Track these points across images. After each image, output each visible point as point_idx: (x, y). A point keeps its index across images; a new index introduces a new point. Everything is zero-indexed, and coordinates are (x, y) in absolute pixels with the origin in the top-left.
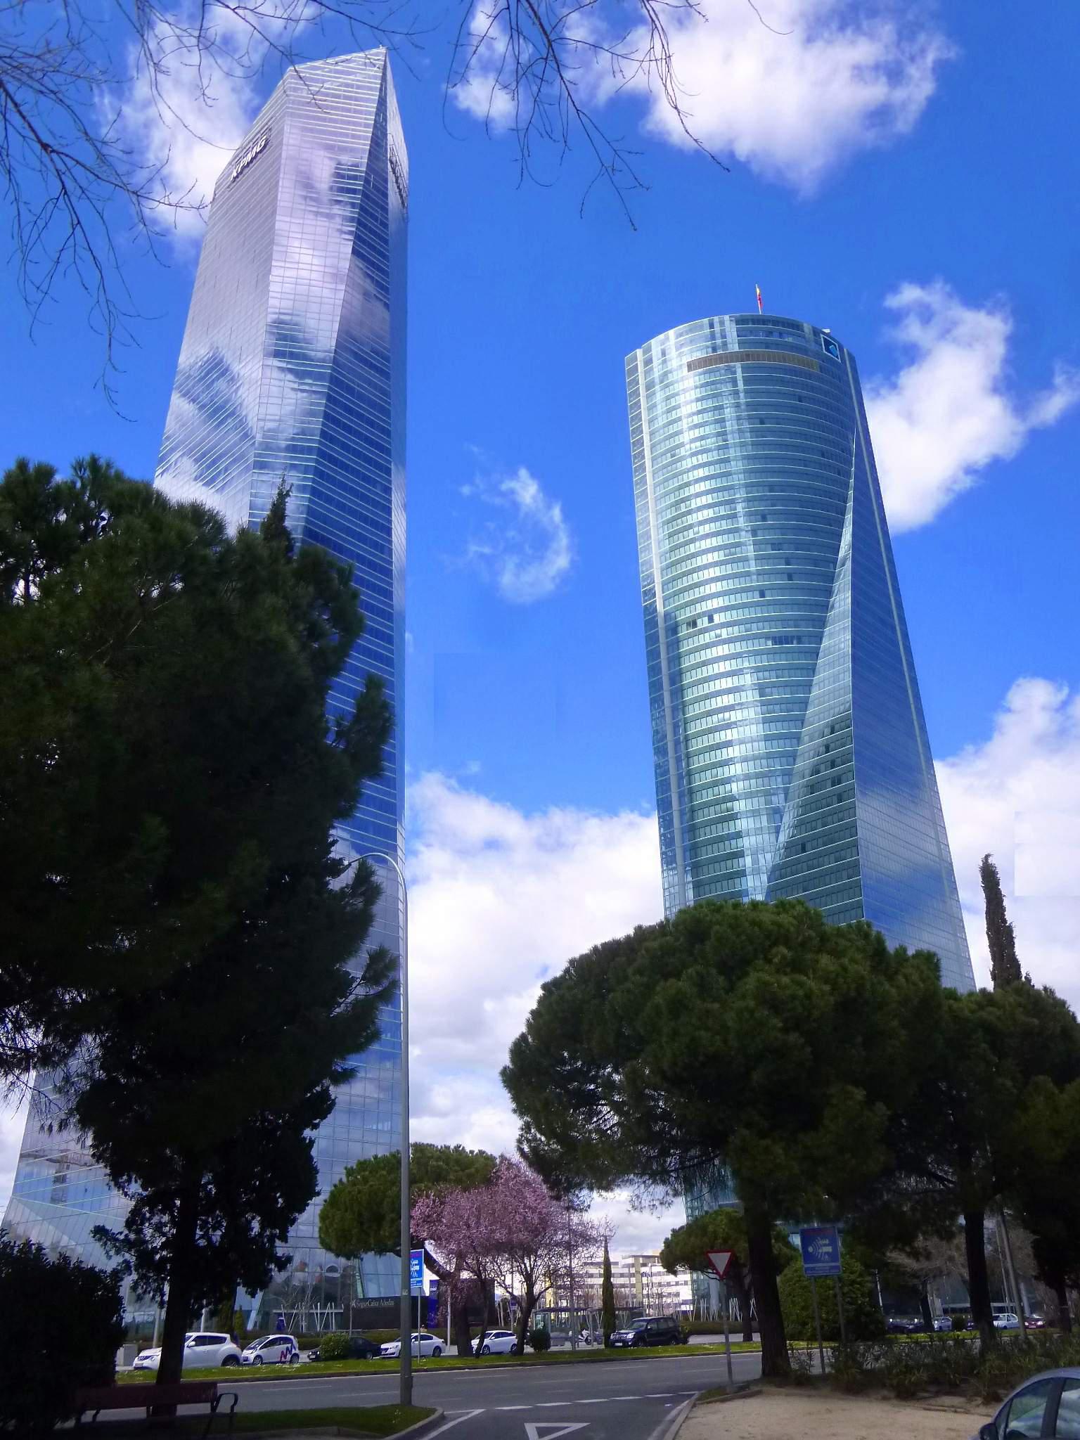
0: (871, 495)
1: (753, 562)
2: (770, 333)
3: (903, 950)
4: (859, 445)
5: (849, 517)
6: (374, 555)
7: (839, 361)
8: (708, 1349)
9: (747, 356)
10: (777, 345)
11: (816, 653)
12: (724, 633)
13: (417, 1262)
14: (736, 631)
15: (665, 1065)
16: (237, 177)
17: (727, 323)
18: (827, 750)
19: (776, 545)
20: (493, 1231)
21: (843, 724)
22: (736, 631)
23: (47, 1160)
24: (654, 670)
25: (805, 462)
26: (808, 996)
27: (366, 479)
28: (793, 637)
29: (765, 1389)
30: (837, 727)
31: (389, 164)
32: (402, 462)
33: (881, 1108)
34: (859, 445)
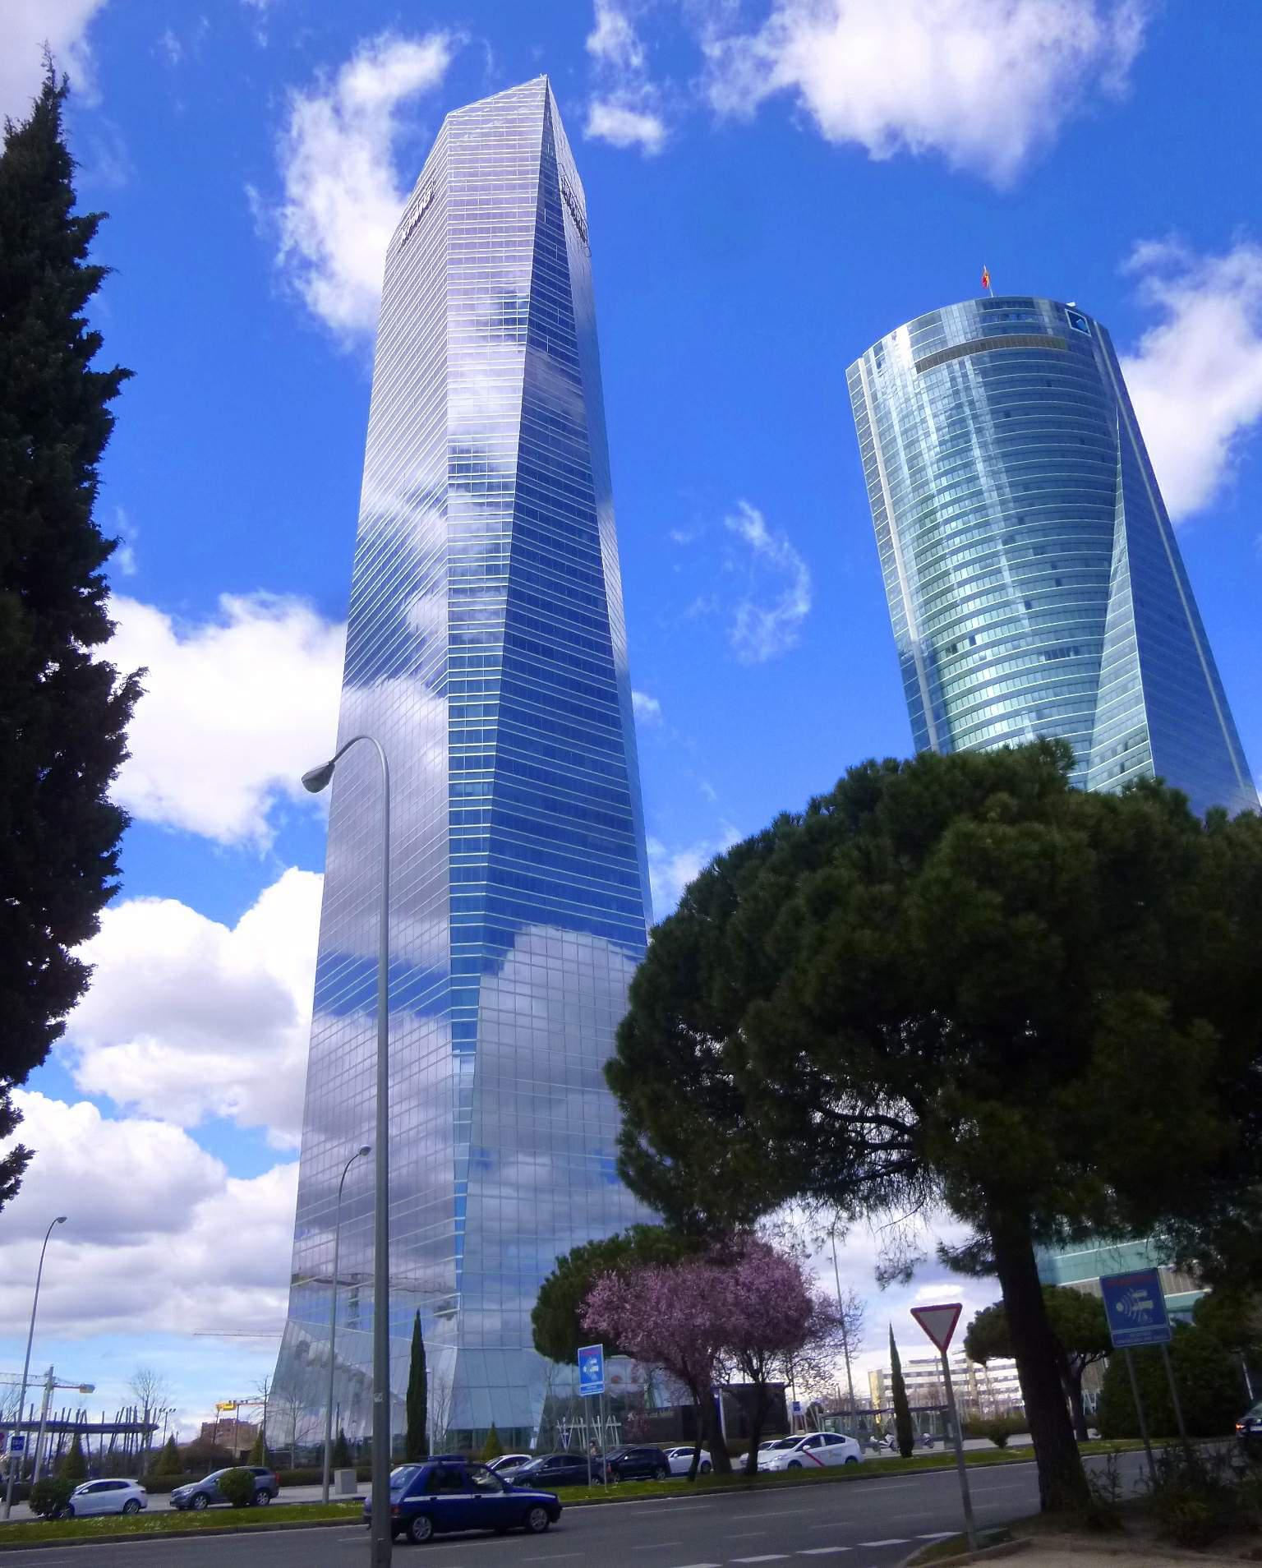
0: (1138, 465)
1: (1026, 622)
2: (1006, 316)
3: (1221, 814)
4: (1123, 426)
5: (1120, 506)
6: (586, 609)
7: (1090, 335)
8: (1015, 1456)
9: (983, 346)
10: (1016, 328)
11: (1098, 664)
12: (989, 654)
13: (595, 1361)
14: (1002, 650)
15: (808, 999)
16: (407, 239)
17: (968, 365)
18: (1123, 770)
19: (1039, 549)
20: (691, 1316)
21: (1137, 738)
22: (1002, 650)
23: (316, 1280)
24: (915, 706)
25: (1064, 453)
26: (1048, 853)
27: (572, 530)
28: (1068, 649)
29: (1036, 1540)
30: (1131, 742)
31: (562, 196)
32: (609, 491)
33: (1204, 1029)
34: (1123, 426)
